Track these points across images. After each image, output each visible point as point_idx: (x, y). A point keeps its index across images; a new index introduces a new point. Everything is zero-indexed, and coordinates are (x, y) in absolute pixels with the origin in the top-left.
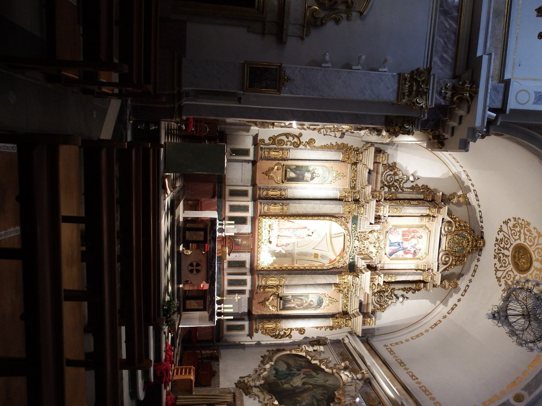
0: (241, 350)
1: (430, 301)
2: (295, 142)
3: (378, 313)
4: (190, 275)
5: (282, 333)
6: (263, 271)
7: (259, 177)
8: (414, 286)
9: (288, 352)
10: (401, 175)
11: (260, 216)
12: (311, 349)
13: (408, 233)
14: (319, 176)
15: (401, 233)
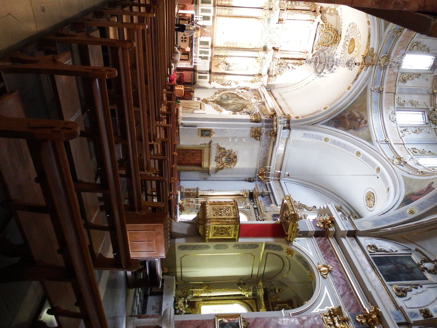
0: (205, 90)
3: (278, 76)
4: (182, 43)
5: (226, 83)
6: (217, 47)
8: (298, 61)
9: (229, 92)
11: (217, 16)
12: (240, 91)
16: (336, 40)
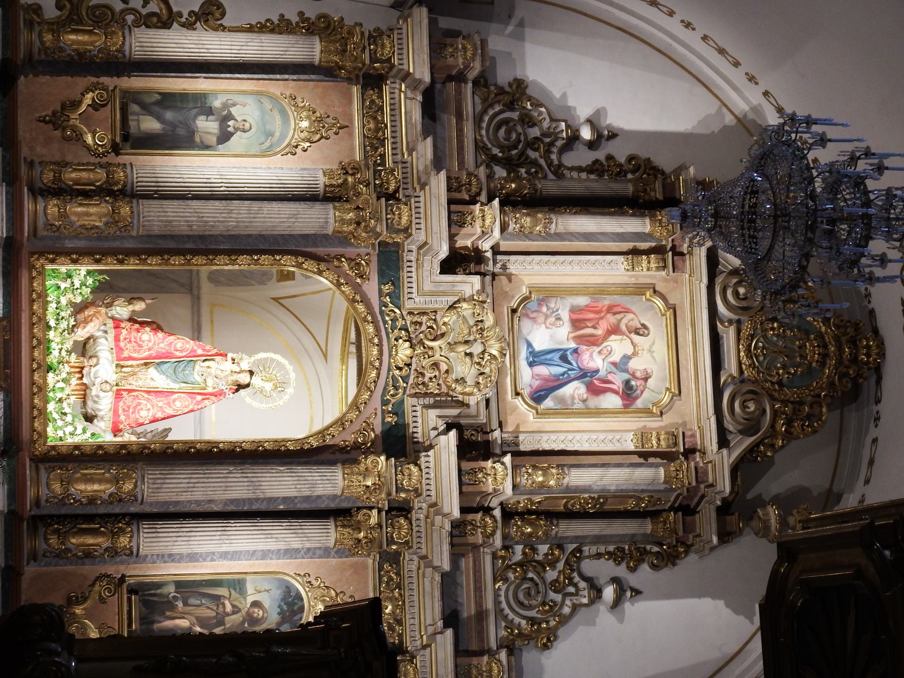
1: (728, 605)
2: (154, 14)
7: (28, 135)
10: (546, 124)
13: (591, 316)
14: (247, 126)
15: (565, 315)
16: (854, 360)
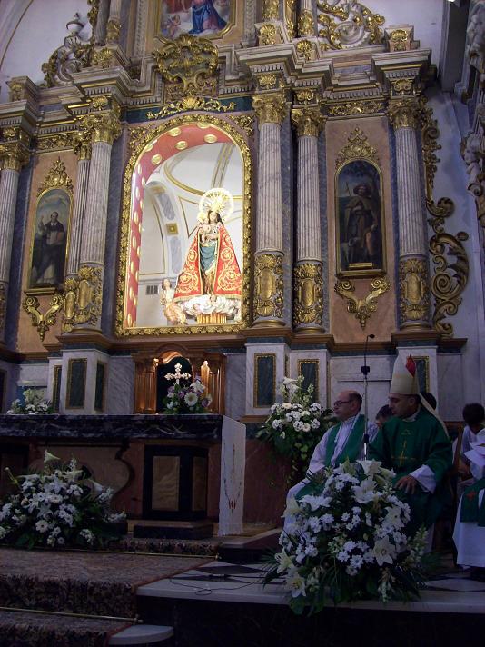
10: (68, 50)
15: (173, 15)
